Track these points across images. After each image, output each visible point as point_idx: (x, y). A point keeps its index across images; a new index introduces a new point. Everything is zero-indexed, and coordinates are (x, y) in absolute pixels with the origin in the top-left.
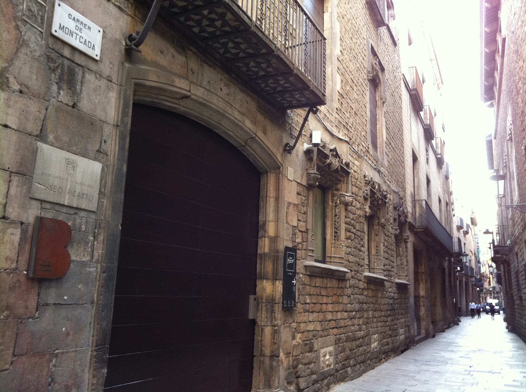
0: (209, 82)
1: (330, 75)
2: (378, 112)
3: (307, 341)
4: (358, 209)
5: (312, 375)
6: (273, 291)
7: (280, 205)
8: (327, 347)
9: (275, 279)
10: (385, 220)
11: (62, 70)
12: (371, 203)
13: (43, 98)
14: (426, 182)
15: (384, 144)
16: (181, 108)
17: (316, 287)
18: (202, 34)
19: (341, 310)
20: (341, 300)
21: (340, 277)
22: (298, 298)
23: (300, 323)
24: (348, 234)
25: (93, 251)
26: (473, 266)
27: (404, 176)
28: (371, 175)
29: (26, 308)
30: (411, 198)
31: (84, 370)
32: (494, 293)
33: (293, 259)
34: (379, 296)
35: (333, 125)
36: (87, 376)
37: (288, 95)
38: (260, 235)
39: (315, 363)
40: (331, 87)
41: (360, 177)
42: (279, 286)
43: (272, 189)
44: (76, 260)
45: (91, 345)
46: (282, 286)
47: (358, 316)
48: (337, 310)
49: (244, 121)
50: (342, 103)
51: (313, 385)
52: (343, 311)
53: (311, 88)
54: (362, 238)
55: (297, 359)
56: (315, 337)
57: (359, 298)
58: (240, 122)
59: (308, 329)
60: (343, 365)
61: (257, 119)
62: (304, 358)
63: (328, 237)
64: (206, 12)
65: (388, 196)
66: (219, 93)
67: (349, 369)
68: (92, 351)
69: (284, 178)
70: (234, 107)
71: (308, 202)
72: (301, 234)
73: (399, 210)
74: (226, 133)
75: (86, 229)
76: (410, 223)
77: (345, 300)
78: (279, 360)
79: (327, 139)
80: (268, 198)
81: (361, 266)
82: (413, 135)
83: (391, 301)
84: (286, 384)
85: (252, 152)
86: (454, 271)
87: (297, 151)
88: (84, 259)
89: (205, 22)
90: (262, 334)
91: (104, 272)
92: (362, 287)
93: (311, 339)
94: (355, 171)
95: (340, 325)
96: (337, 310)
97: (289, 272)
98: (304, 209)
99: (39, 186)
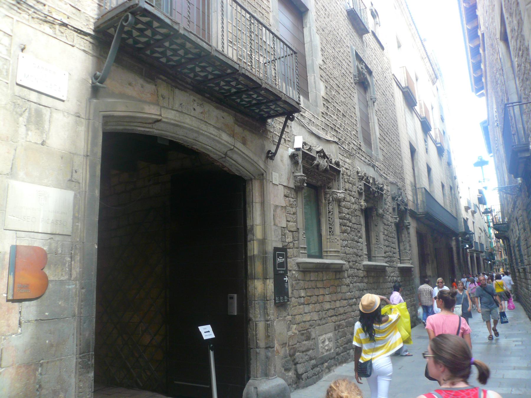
0: (181, 104)
1: (313, 83)
2: (370, 111)
3: (304, 330)
4: (353, 204)
5: (311, 360)
6: (264, 289)
7: (265, 209)
8: (326, 334)
9: (265, 278)
10: (383, 211)
11: (30, 113)
12: (365, 196)
13: (12, 140)
14: (426, 170)
15: (378, 140)
16: (155, 131)
17: (311, 281)
18: (170, 63)
19: (339, 299)
20: (339, 290)
21: (338, 270)
22: (292, 293)
23: (295, 315)
24: (344, 228)
25: (71, 270)
26: (483, 242)
27: (402, 167)
28: (365, 170)
29: (9, 326)
30: (412, 186)
31: (70, 376)
32: (506, 264)
33: (283, 258)
34: (381, 281)
35: (320, 128)
36: (73, 381)
37: (263, 107)
38: (249, 239)
39: (313, 349)
40: (315, 94)
41: (353, 173)
42: (270, 284)
43: (257, 194)
44: (54, 279)
45: (75, 353)
46: (273, 285)
48: (335, 299)
49: (220, 135)
50: (328, 107)
51: (312, 369)
52: (342, 299)
53: (283, 98)
54: (359, 230)
55: (294, 348)
56: (312, 326)
57: (359, 286)
58: (217, 136)
59: (304, 320)
60: (344, 348)
61: (235, 131)
62: (301, 347)
63: (324, 233)
64: (167, 44)
65: (385, 187)
66: (193, 113)
67: (352, 350)
68: (76, 358)
69: (268, 184)
70: (209, 124)
71: (297, 202)
72: (290, 233)
73: (397, 200)
74: (205, 148)
75: (62, 251)
76: (411, 210)
77: (344, 289)
78: (274, 351)
79: (312, 141)
80: (254, 204)
81: (360, 256)
82: (408, 128)
84: (283, 371)
85: (233, 162)
86: (463, 249)
87: (282, 157)
88: (62, 278)
89: (169, 53)
90: (256, 329)
91: (83, 288)
92: (362, 275)
93: (308, 329)
94: (347, 169)
95: (339, 313)
96: (335, 299)
97: (280, 270)
99: (13, 218)
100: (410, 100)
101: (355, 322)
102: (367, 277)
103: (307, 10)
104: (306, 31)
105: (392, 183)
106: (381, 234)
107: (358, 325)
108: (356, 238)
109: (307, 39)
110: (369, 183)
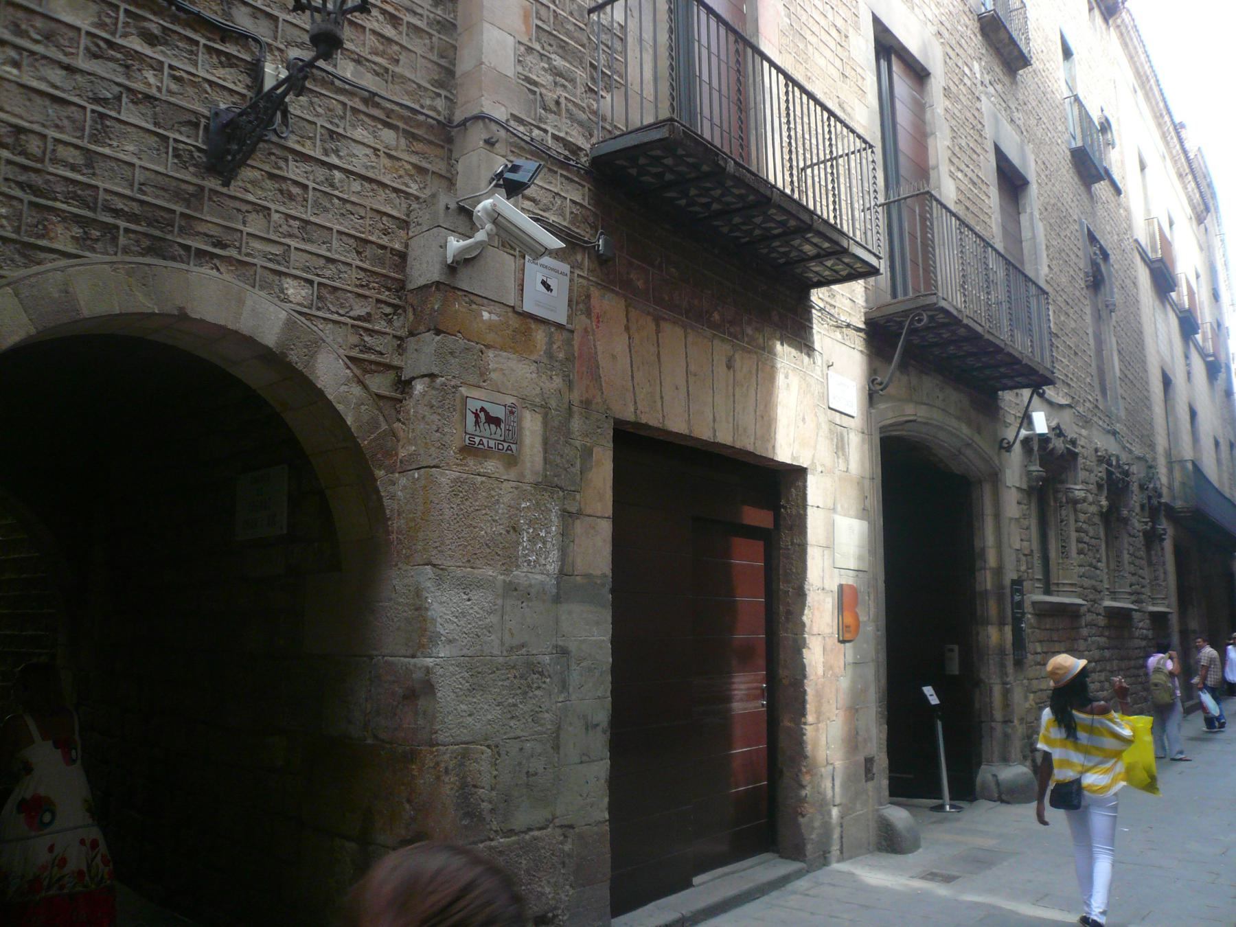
9: (1002, 624)
14: (1188, 417)
15: (1118, 382)
24: (1081, 545)
41: (1088, 452)
47: (1099, 668)
63: (1053, 554)
76: (1166, 504)
83: (1144, 643)
98: (1026, 523)
100: (1164, 280)
101: (1041, 709)
102: (1107, 627)
103: (928, 74)
104: (1024, 219)
105: (1139, 458)
106: (1125, 552)
107: (1047, 713)
108: (1094, 561)
109: (1026, 234)
110: (1111, 465)
